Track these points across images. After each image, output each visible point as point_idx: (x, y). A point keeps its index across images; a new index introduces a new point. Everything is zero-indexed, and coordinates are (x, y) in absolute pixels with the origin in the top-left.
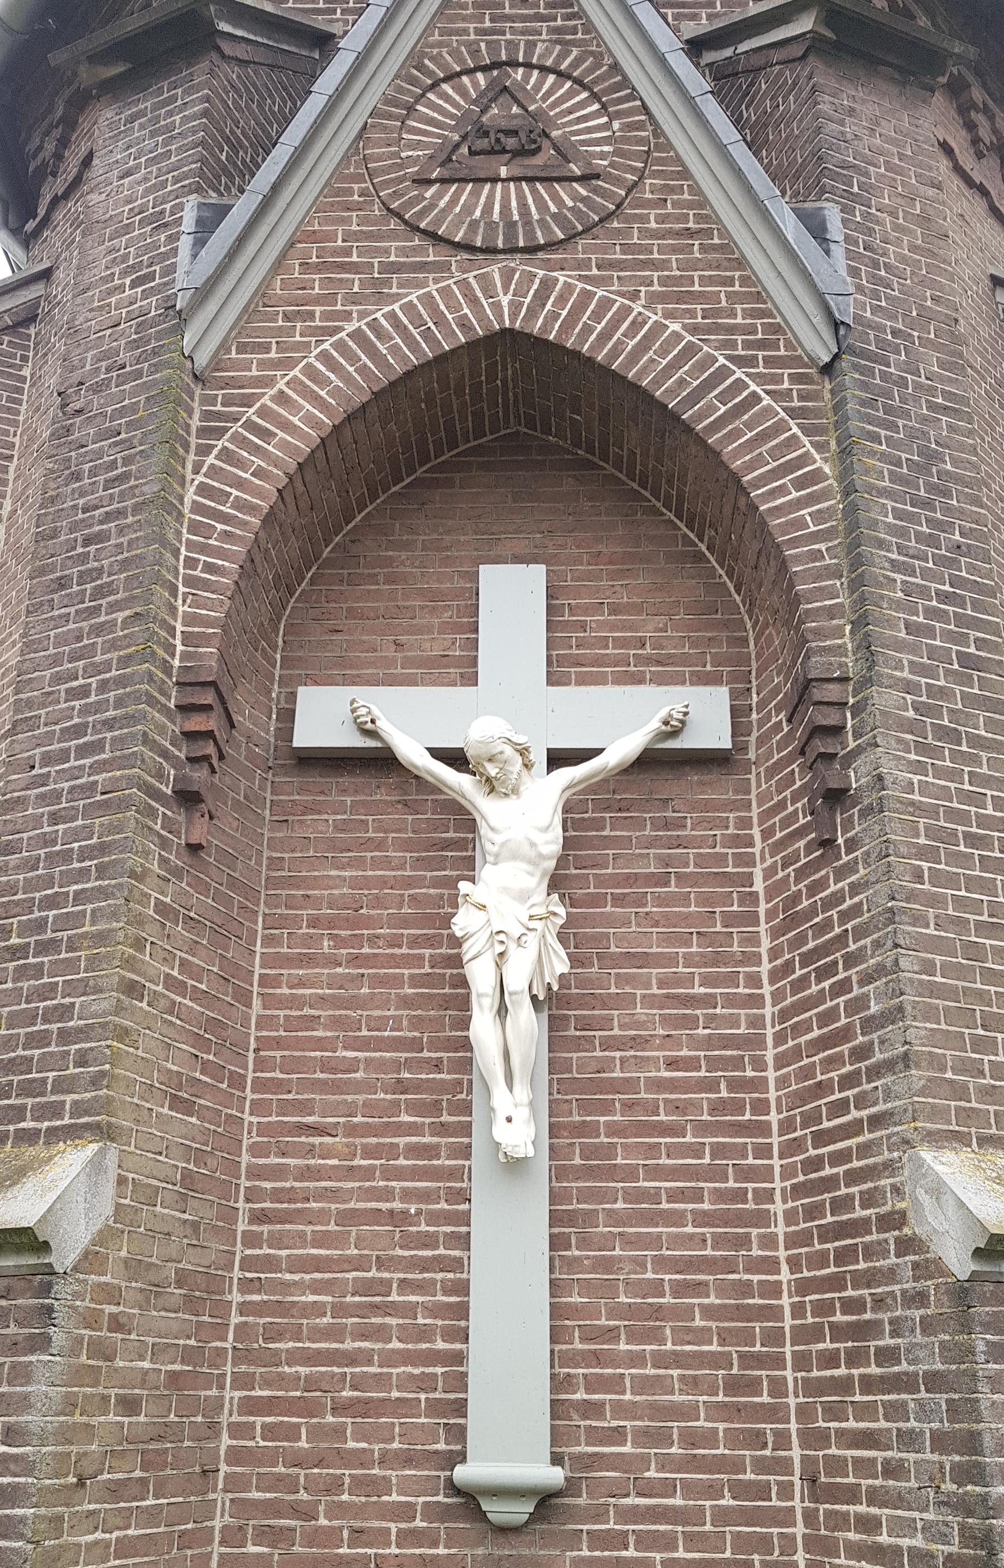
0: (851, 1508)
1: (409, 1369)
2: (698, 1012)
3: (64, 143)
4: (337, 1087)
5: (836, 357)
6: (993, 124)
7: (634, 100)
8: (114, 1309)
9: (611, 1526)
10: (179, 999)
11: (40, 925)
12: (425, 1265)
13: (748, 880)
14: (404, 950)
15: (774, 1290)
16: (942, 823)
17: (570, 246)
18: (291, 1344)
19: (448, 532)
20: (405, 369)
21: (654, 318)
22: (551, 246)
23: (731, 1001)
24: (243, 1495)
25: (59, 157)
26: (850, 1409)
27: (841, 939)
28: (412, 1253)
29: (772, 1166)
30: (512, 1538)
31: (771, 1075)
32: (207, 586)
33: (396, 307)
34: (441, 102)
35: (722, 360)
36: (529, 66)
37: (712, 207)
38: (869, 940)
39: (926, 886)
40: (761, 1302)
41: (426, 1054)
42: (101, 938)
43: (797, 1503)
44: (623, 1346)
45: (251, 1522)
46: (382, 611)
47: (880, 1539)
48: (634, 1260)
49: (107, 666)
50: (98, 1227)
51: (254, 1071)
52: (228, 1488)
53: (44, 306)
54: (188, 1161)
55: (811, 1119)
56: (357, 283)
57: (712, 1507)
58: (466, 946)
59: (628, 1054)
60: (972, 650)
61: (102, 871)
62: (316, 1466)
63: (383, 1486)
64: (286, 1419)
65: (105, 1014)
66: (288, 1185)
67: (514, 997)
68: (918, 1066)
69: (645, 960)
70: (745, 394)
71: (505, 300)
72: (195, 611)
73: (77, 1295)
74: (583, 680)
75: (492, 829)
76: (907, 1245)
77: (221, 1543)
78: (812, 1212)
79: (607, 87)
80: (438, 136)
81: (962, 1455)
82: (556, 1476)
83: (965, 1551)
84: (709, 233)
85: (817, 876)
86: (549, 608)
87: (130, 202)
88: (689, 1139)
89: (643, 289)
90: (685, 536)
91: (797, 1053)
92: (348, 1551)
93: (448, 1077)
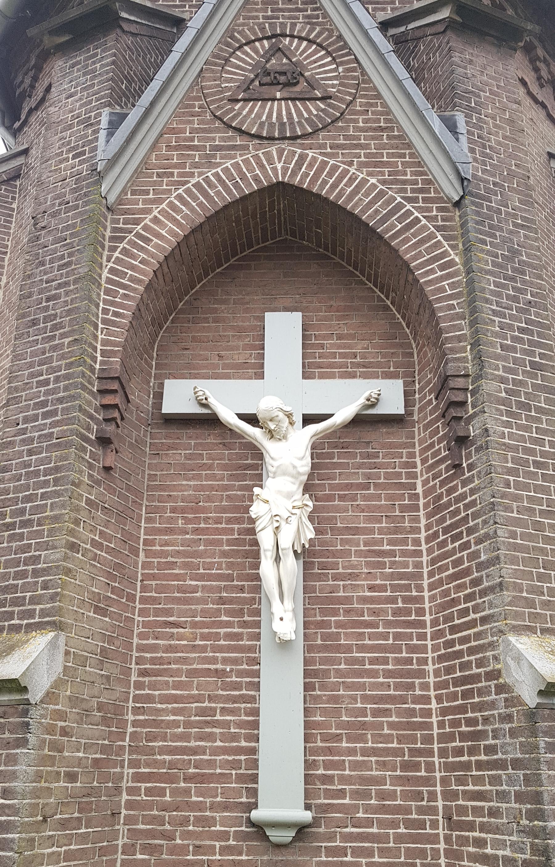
0: (471, 834)
1: (226, 757)
2: (386, 560)
3: (35, 79)
4: (186, 601)
5: (462, 197)
6: (549, 68)
7: (351, 55)
8: (63, 724)
9: (338, 844)
10: (99, 552)
11: (22, 512)
12: (235, 699)
13: (413, 486)
14: (224, 526)
15: (428, 713)
16: (521, 455)
17: (315, 136)
18: (161, 743)
19: (248, 294)
20: (224, 204)
21: (362, 176)
22: (305, 136)
23: (404, 553)
24: (134, 827)
25: (32, 87)
26: (470, 779)
27: (465, 519)
28: (228, 693)
29: (427, 645)
30: (283, 851)
31: (426, 594)
32: (114, 324)
33: (219, 170)
34: (244, 56)
35: (399, 199)
36: (292, 36)
37: (393, 115)
38: (480, 520)
39: (512, 490)
40: (421, 720)
41: (235, 583)
42: (56, 519)
43: (440, 831)
44: (344, 744)
45: (139, 842)
46: (211, 338)
47: (486, 851)
48: (350, 697)
49: (59, 368)
50: (54, 679)
51: (141, 592)
52: (126, 823)
53: (24, 169)
54: (104, 642)
55: (448, 619)
56: (197, 156)
57: (394, 833)
58: (257, 523)
59: (347, 583)
60: (537, 359)
61: (56, 482)
62: (174, 811)
63: (212, 822)
64: (158, 785)
65: (58, 560)
66: (159, 655)
67: (284, 551)
68: (507, 590)
69: (357, 531)
70: (412, 218)
71: (279, 166)
72: (108, 338)
73: (42, 716)
74: (322, 376)
75: (272, 458)
76: (501, 689)
77: (122, 853)
78: (449, 670)
79: (336, 48)
80: (242, 75)
81: (532, 805)
82: (307, 816)
83: (533, 857)
84: (392, 129)
85: (451, 485)
86: (304, 336)
87: (72, 112)
88: (381, 630)
89: (355, 160)
90: (379, 296)
91: (440, 582)
92: (192, 858)
93: (248, 595)
